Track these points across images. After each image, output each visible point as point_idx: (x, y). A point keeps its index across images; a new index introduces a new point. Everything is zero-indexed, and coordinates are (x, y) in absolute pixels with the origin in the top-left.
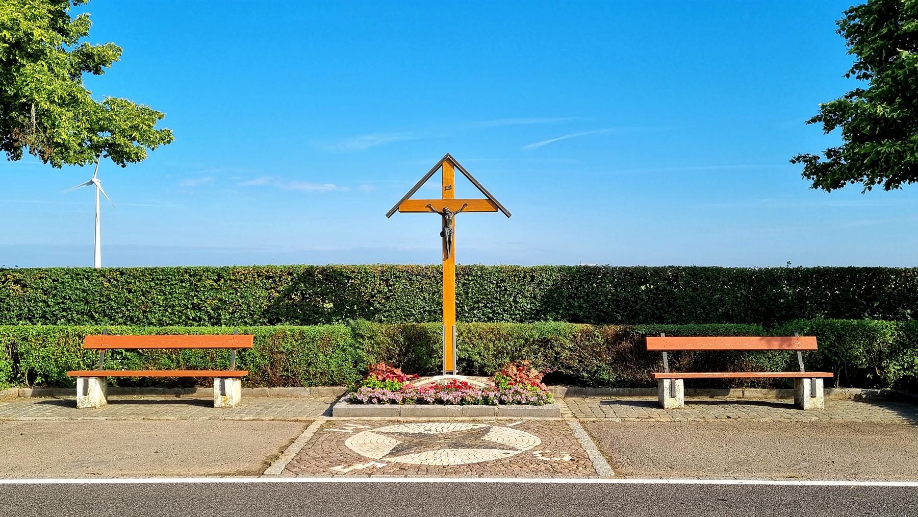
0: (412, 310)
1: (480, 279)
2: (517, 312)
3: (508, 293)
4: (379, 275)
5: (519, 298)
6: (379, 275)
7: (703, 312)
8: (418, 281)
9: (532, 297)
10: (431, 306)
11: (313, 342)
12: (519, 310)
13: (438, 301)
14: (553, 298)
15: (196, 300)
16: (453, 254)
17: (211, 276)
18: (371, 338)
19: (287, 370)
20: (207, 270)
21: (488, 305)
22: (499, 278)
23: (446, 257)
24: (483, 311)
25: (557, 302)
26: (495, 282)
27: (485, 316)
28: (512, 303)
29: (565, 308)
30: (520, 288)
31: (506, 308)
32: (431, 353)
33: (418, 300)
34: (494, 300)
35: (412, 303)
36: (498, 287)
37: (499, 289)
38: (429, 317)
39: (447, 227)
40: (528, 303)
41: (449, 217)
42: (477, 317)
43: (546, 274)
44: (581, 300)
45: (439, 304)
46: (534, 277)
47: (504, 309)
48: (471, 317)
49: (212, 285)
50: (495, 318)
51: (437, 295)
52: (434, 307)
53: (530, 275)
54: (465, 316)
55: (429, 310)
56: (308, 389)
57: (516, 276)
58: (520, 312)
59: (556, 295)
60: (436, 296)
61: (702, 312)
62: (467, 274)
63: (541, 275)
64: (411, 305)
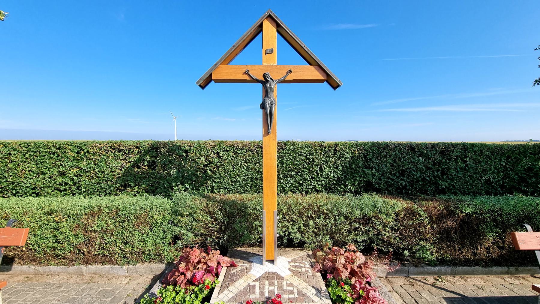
0: (237, 177)
1: (293, 153)
2: (323, 179)
3: (315, 163)
4: (211, 149)
5: (324, 168)
6: (211, 149)
7: (470, 180)
8: (242, 154)
9: (335, 167)
10: (253, 174)
11: (128, 220)
12: (324, 177)
13: (259, 170)
14: (351, 168)
15: (61, 169)
16: (274, 129)
17: (73, 149)
18: (190, 215)
19: (103, 248)
20: (71, 144)
21: (299, 174)
22: (308, 152)
23: (267, 132)
24: (295, 178)
25: (355, 171)
26: (305, 155)
27: (296, 182)
28: (318, 172)
29: (360, 177)
30: (324, 160)
31: (313, 176)
32: (251, 229)
33: (243, 169)
34: (304, 170)
35: (237, 172)
36: (307, 159)
37: (308, 161)
38: (251, 183)
39: (268, 97)
40: (331, 172)
41: (270, 85)
42: (290, 183)
43: (346, 148)
44: (374, 170)
45: (260, 172)
46: (337, 150)
47: (312, 177)
48: (286, 183)
49: (74, 157)
50: (304, 184)
51: (257, 165)
52: (256, 175)
53: (335, 148)
54: (281, 182)
55: (251, 178)
56: (125, 267)
57: (321, 150)
58: (325, 179)
59: (353, 166)
60: (257, 166)
61: (469, 179)
62: (282, 148)
63: (342, 149)
64: (237, 173)
